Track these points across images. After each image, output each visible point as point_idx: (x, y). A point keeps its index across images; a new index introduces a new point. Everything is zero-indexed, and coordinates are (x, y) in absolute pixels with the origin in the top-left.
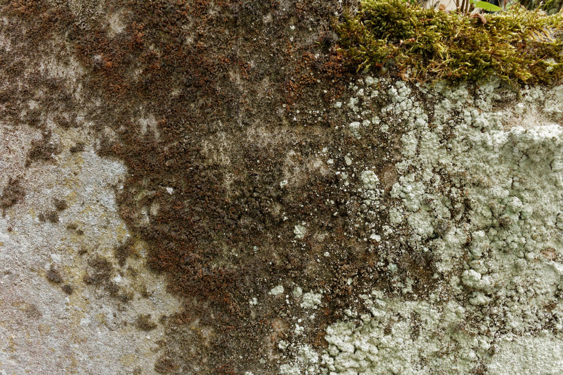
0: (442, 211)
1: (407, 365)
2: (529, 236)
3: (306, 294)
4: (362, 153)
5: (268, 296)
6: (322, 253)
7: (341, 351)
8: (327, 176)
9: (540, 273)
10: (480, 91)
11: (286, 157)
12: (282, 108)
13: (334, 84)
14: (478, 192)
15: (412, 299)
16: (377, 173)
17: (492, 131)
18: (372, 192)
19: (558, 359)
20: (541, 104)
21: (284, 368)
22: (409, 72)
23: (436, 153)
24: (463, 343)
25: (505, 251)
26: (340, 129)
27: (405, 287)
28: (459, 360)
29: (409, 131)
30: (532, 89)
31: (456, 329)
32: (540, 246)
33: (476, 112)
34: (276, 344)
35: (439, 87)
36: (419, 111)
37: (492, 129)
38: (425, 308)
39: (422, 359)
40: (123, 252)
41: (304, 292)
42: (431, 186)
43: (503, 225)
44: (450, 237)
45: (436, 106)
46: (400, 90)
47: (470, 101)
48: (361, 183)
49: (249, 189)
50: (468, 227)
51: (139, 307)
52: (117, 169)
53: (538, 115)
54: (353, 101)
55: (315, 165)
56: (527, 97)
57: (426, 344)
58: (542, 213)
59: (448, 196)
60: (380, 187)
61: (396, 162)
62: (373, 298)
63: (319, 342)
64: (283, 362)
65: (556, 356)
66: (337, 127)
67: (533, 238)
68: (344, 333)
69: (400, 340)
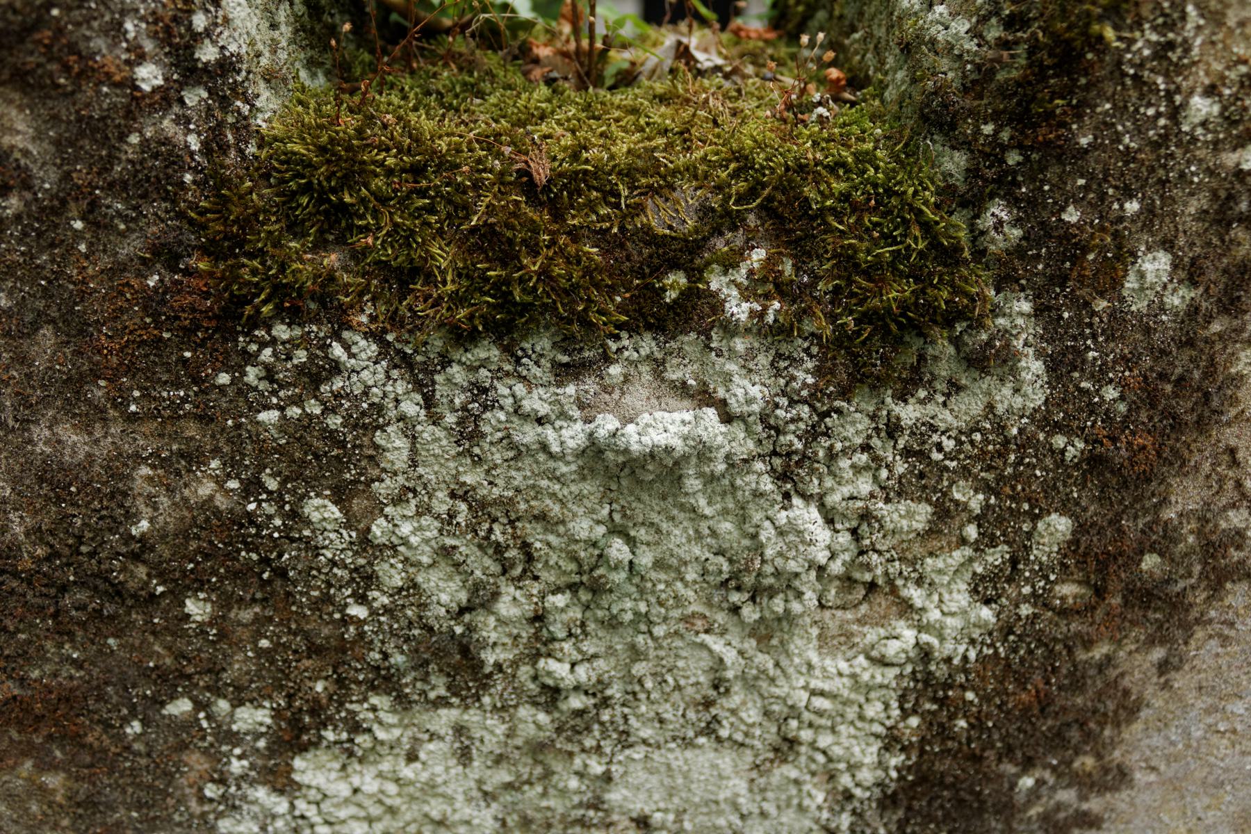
0: (482, 565)
1: (458, 805)
2: (653, 600)
3: (238, 710)
4: (295, 467)
5: (164, 717)
6: (255, 643)
7: (325, 796)
8: (231, 511)
9: (684, 654)
10: (523, 349)
11: (133, 479)
12: (99, 387)
13: (203, 340)
14: (546, 530)
15: (449, 705)
16: (335, 503)
17: (558, 423)
18: (333, 536)
19: (728, 778)
20: (658, 366)
21: (224, 825)
22: (369, 310)
23: (452, 465)
24: (557, 766)
25: (613, 624)
26: (238, 426)
27: (432, 689)
28: (552, 791)
29: (388, 424)
30: (637, 338)
31: (537, 749)
32: (676, 613)
33: (520, 389)
34: (201, 790)
35: (437, 343)
36: (401, 387)
37: (558, 418)
38: (475, 719)
39: (486, 794)
41: (234, 706)
42: (450, 524)
43: (597, 589)
44: (504, 607)
45: (437, 378)
46: (354, 350)
47: (507, 367)
48: (308, 523)
50: (535, 588)
53: (655, 385)
54: (252, 374)
55: (200, 492)
56: (626, 354)
57: (489, 772)
58: (674, 561)
59: (487, 538)
60: (348, 526)
61: (373, 481)
62: (374, 709)
63: (284, 784)
64: (220, 815)
65: (725, 774)
66: (230, 422)
67: (661, 604)
68: (329, 765)
69: (439, 769)
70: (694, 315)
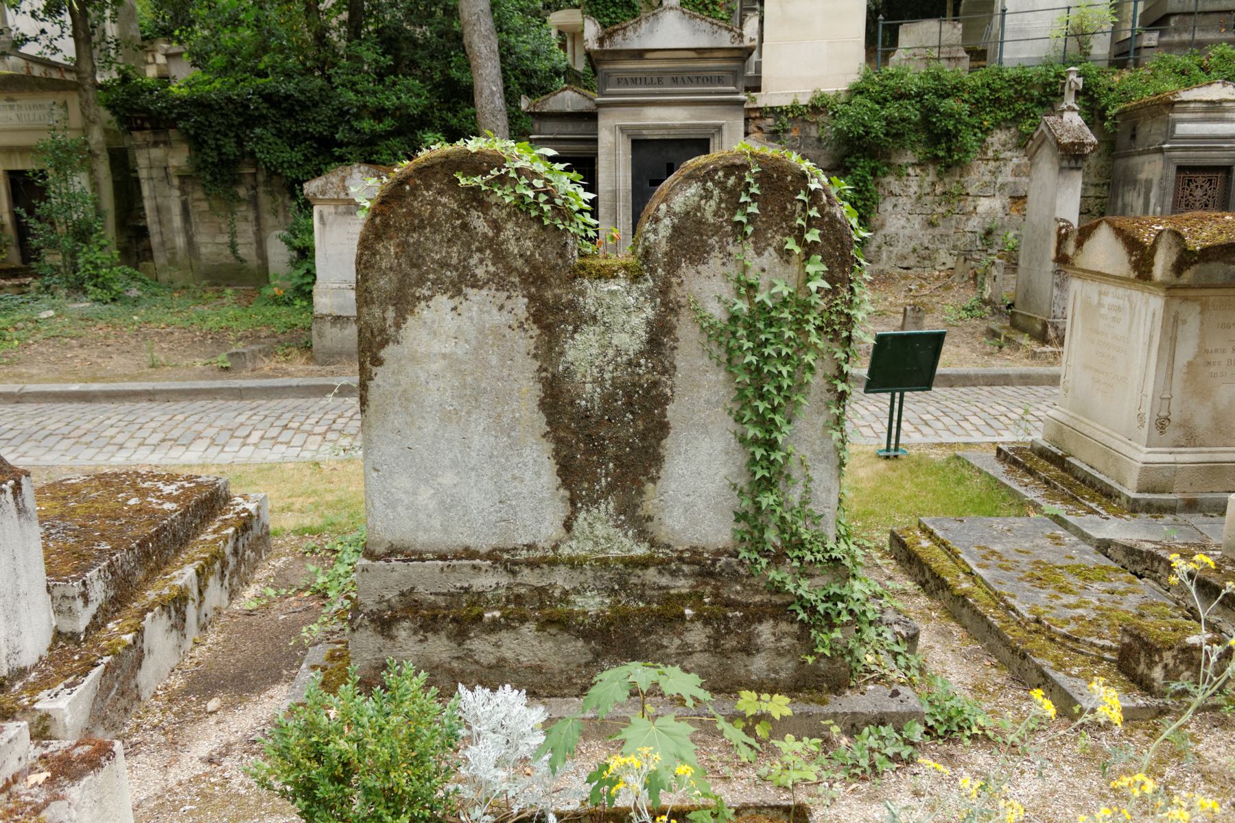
40: (527, 319)
49: (556, 302)
51: (531, 333)
52: (526, 300)
63: (573, 338)
70: (617, 276)
